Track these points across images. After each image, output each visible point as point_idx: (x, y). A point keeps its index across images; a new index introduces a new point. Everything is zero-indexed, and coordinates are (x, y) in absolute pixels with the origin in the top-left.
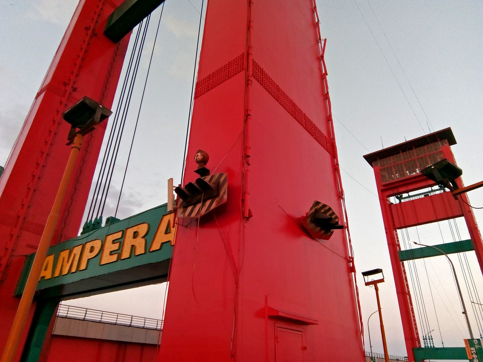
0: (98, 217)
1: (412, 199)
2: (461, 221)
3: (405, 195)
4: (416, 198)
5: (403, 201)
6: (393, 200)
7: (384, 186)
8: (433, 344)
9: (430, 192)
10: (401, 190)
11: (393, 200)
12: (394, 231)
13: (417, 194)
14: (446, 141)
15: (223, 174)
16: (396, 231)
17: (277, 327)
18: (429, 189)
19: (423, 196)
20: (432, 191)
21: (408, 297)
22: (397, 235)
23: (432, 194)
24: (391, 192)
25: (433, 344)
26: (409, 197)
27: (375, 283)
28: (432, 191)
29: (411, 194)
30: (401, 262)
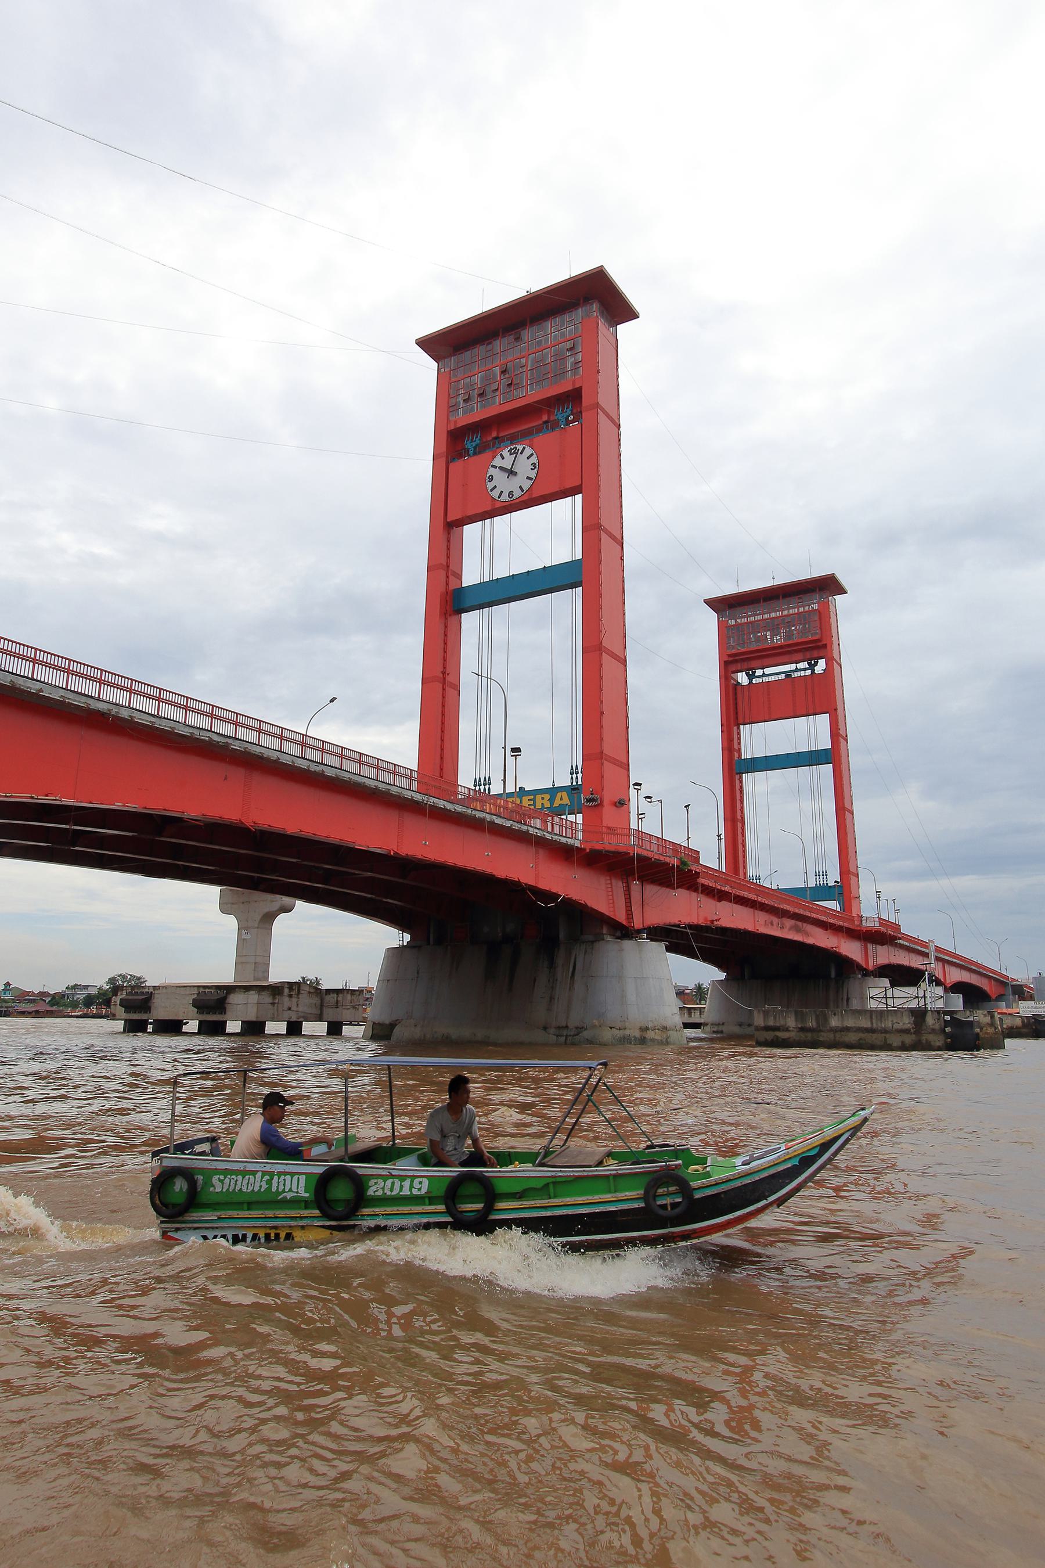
0: (587, 1370)
1: (766, 679)
2: (824, 719)
3: (759, 672)
4: (774, 678)
5: (754, 681)
6: (742, 678)
7: (729, 656)
8: (572, 778)
9: (793, 671)
10: (753, 664)
11: (742, 678)
12: (735, 728)
13: (775, 672)
14: (595, 306)
15: (703, 885)
16: (739, 728)
17: (458, 1086)
18: (793, 667)
19: (783, 677)
20: (797, 670)
21: (739, 825)
22: (739, 733)
23: (795, 675)
24: (739, 666)
25: (572, 778)
26: (764, 675)
27: (638, 790)
28: (797, 670)
29: (768, 671)
30: (737, 777)
